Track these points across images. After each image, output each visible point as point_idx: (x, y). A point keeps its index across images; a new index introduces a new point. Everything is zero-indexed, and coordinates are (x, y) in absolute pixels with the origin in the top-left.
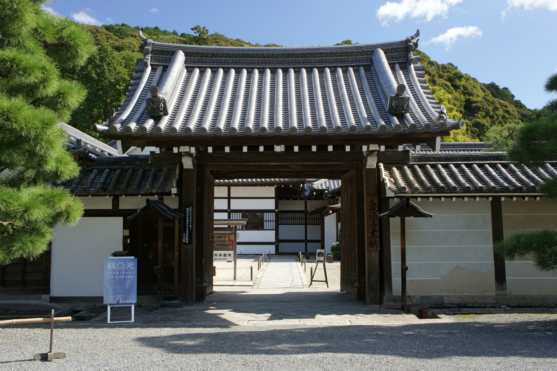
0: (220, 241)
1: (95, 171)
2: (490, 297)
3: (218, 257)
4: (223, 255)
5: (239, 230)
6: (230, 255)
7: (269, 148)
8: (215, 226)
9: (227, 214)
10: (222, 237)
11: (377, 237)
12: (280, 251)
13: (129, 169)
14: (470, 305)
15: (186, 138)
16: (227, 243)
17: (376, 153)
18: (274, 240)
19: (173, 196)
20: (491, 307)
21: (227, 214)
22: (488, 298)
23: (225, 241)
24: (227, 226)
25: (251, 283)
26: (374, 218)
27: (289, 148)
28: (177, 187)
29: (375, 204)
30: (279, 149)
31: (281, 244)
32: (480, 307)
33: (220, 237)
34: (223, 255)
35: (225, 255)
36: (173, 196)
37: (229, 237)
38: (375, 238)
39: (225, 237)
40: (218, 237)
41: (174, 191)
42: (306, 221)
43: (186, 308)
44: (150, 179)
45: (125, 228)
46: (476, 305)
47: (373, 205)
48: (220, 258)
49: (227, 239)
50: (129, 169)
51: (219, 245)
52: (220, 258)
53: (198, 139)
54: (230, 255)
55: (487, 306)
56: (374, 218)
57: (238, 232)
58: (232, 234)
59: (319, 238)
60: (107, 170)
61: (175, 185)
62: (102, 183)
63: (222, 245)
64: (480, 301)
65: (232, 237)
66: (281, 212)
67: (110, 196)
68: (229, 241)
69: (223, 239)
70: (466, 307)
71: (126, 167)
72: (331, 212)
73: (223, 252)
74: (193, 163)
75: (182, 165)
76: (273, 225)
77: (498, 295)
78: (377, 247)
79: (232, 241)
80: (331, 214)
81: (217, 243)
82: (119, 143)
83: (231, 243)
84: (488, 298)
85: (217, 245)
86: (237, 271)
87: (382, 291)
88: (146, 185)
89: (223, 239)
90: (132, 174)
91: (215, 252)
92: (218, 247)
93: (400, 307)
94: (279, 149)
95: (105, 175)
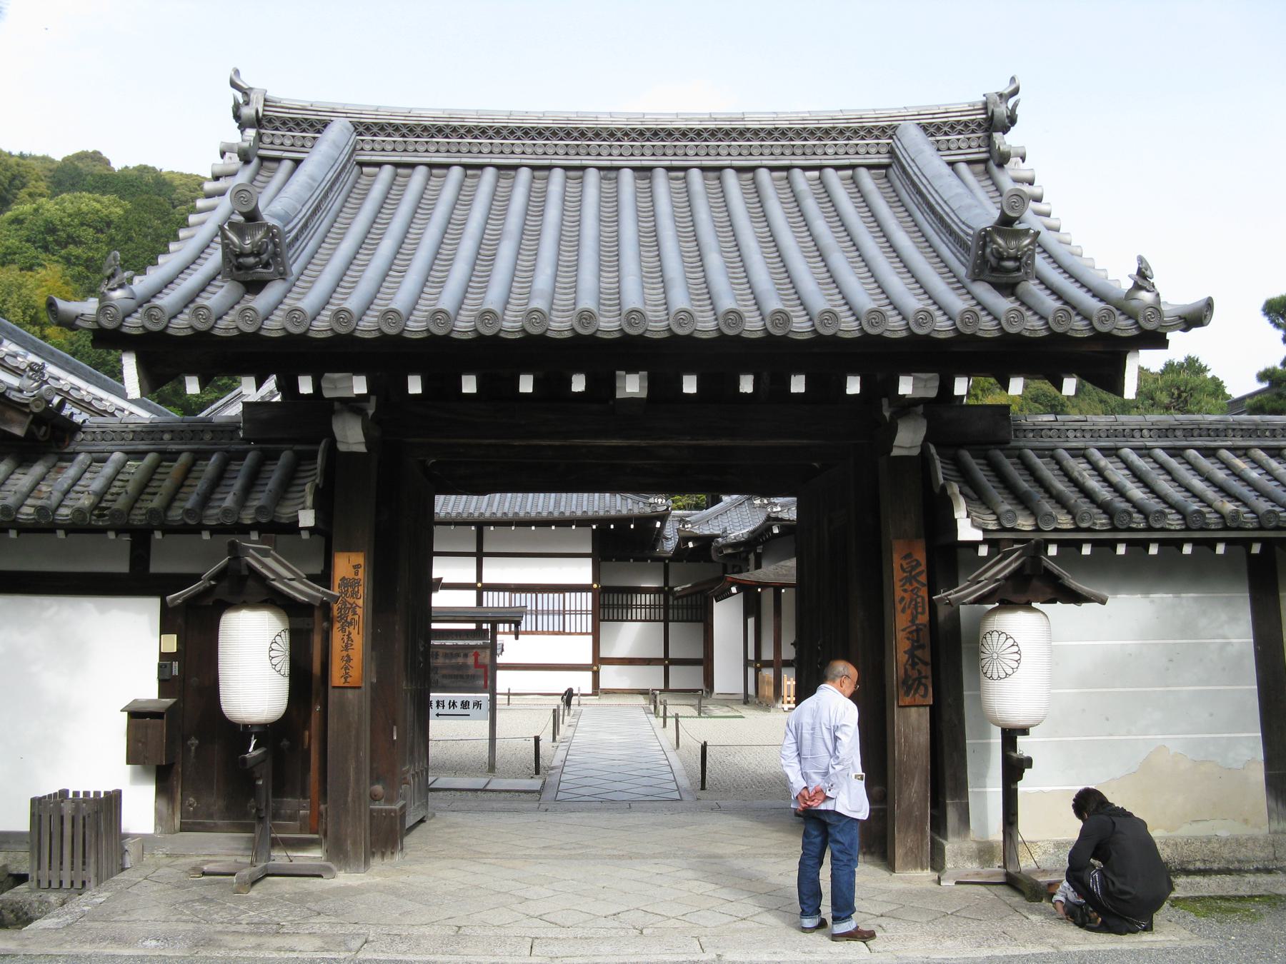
0: (453, 667)
1: (81, 457)
2: (1254, 840)
3: (447, 710)
4: (458, 704)
5: (504, 633)
6: (478, 704)
7: (603, 385)
8: (435, 626)
9: (473, 593)
10: (458, 655)
11: (925, 664)
12: (603, 684)
13: (179, 453)
14: (1199, 865)
15: (342, 351)
16: (472, 671)
17: (920, 409)
18: (590, 661)
19: (305, 535)
20: (1258, 870)
21: (473, 593)
22: (1250, 844)
23: (465, 666)
24: (472, 626)
25: (536, 783)
26: (916, 607)
27: (663, 387)
28: (316, 506)
29: (918, 564)
30: (632, 386)
31: (605, 670)
32: (1228, 872)
33: (451, 656)
34: (458, 704)
35: (465, 705)
36: (305, 535)
37: (476, 655)
38: (920, 666)
39: (466, 656)
40: (446, 656)
41: (307, 519)
42: (666, 614)
43: (344, 878)
44: (238, 484)
45: (165, 629)
46: (1215, 866)
47: (913, 568)
48: (452, 711)
49: (471, 661)
50: (179, 453)
51: (450, 676)
52: (452, 711)
53: (385, 354)
54: (478, 704)
55: (1246, 867)
56: (916, 607)
57: (499, 637)
58: (483, 647)
59: (699, 654)
60: (117, 456)
61: (309, 500)
62: (95, 493)
63: (456, 677)
64: (1226, 853)
65: (485, 657)
66: (606, 590)
67: (119, 531)
68: (477, 665)
69: (460, 660)
70: (1188, 873)
71: (174, 447)
72: (734, 590)
73: (459, 697)
74: (365, 435)
75: (333, 441)
76: (587, 622)
77: (1276, 832)
78: (925, 696)
79: (485, 666)
80: (985, 560)
81: (445, 672)
82: (129, 364)
83: (481, 671)
84: (1250, 844)
85: (444, 676)
86: (499, 715)
87: (939, 825)
88: (224, 499)
89: (460, 660)
90: (188, 471)
91: (434, 696)
92: (446, 682)
93: (1001, 879)
94: (632, 386)
95: (108, 469)
